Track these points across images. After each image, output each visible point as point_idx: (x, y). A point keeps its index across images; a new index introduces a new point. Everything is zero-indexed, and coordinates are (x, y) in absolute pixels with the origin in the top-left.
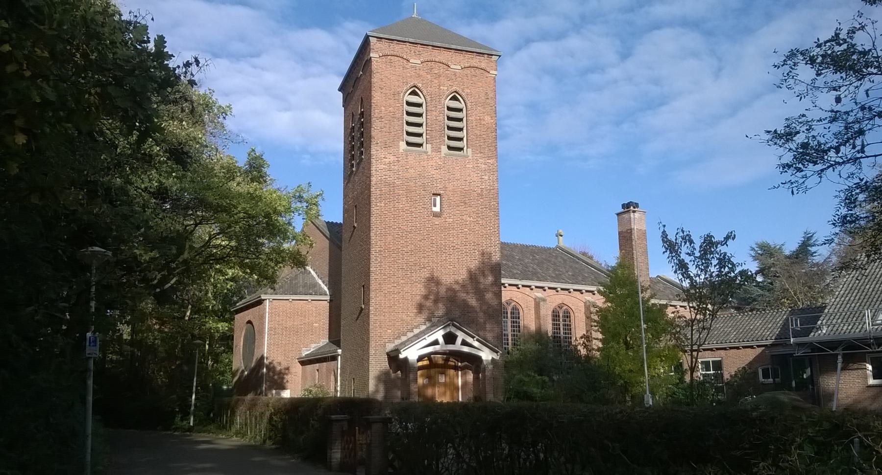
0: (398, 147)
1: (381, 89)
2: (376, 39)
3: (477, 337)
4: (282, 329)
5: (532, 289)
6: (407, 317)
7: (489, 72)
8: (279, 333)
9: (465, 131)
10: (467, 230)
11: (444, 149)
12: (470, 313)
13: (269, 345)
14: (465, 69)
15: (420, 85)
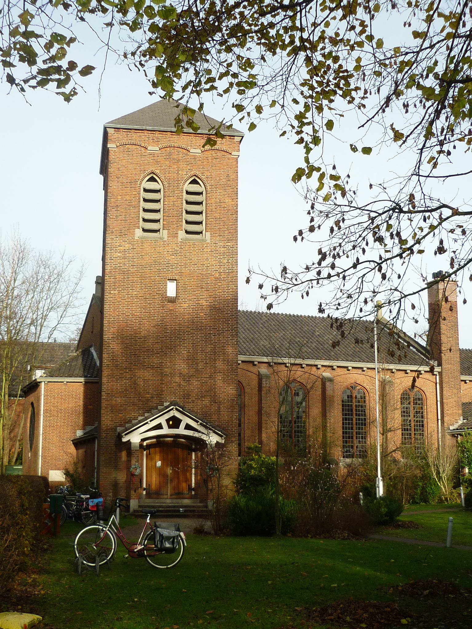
0: (134, 234)
1: (118, 178)
2: (113, 129)
3: (200, 421)
4: (57, 412)
5: (318, 369)
6: (139, 401)
7: (231, 154)
8: (54, 416)
9: (204, 214)
10: (203, 314)
11: (182, 234)
12: (204, 397)
13: (45, 427)
14: (206, 153)
15: (158, 172)
